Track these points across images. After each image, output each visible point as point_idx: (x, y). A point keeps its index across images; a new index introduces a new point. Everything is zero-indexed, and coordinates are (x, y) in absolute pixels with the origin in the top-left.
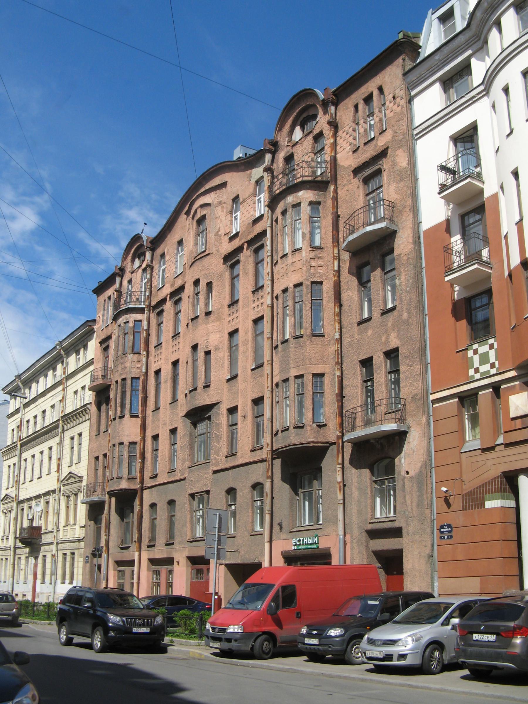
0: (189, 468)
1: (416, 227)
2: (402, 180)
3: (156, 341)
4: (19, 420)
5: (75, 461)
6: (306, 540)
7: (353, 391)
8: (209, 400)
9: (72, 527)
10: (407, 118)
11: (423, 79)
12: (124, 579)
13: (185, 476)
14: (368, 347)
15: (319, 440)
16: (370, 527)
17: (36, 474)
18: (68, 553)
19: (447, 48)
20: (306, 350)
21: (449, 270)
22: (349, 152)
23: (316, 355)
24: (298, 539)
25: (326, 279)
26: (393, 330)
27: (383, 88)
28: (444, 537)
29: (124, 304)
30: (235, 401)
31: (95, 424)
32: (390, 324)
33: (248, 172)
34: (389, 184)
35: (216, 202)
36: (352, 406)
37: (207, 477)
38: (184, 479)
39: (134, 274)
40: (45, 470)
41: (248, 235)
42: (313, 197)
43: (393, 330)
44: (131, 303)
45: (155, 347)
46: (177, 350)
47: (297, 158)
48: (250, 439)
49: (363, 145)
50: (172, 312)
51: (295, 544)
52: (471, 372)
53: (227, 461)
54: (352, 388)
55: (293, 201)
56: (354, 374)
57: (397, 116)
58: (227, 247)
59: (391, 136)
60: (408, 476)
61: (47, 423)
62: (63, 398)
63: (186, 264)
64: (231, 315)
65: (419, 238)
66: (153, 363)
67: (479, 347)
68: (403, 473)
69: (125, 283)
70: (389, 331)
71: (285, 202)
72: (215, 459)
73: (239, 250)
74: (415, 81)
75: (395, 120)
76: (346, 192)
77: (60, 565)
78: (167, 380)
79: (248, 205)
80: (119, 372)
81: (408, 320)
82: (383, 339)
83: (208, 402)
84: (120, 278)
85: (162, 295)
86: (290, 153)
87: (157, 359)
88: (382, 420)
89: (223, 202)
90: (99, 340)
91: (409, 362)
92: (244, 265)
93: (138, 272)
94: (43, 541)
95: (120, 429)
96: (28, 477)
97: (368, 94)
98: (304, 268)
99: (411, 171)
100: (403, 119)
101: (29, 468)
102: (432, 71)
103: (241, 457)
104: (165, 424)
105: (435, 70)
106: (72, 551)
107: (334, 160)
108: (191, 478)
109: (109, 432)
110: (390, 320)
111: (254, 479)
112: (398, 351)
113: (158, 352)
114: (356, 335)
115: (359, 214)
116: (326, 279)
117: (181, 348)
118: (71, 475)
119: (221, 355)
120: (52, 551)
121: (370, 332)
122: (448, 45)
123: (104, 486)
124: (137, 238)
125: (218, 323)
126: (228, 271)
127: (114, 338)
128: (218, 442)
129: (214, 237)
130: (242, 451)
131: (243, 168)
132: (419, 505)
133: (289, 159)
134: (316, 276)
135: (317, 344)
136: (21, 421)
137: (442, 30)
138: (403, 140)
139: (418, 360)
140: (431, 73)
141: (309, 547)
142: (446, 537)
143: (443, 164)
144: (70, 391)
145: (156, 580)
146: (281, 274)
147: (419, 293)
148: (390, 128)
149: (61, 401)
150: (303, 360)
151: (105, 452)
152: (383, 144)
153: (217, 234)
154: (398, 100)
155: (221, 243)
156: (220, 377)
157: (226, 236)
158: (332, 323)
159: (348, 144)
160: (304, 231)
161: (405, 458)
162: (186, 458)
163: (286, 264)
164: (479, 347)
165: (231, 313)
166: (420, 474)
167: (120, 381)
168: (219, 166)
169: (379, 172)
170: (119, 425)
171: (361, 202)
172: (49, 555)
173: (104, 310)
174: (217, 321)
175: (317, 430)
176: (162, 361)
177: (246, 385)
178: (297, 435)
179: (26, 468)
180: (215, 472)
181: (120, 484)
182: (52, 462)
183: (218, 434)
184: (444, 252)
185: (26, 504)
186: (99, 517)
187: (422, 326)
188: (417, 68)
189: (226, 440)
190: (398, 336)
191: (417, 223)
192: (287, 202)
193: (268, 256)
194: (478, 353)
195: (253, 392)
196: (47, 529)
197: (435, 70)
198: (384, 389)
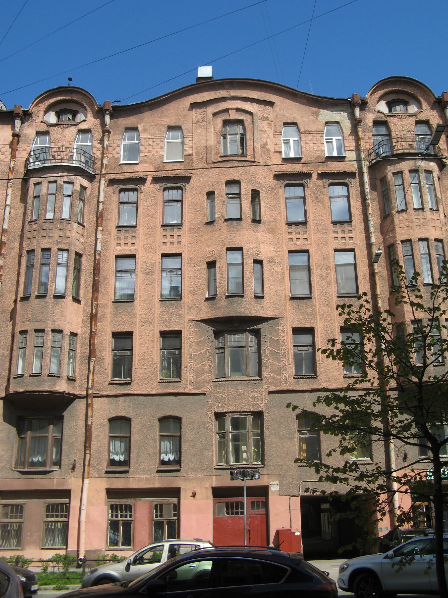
12: (21, 517)
44: (63, 161)
83: (262, 314)
131: (305, 101)
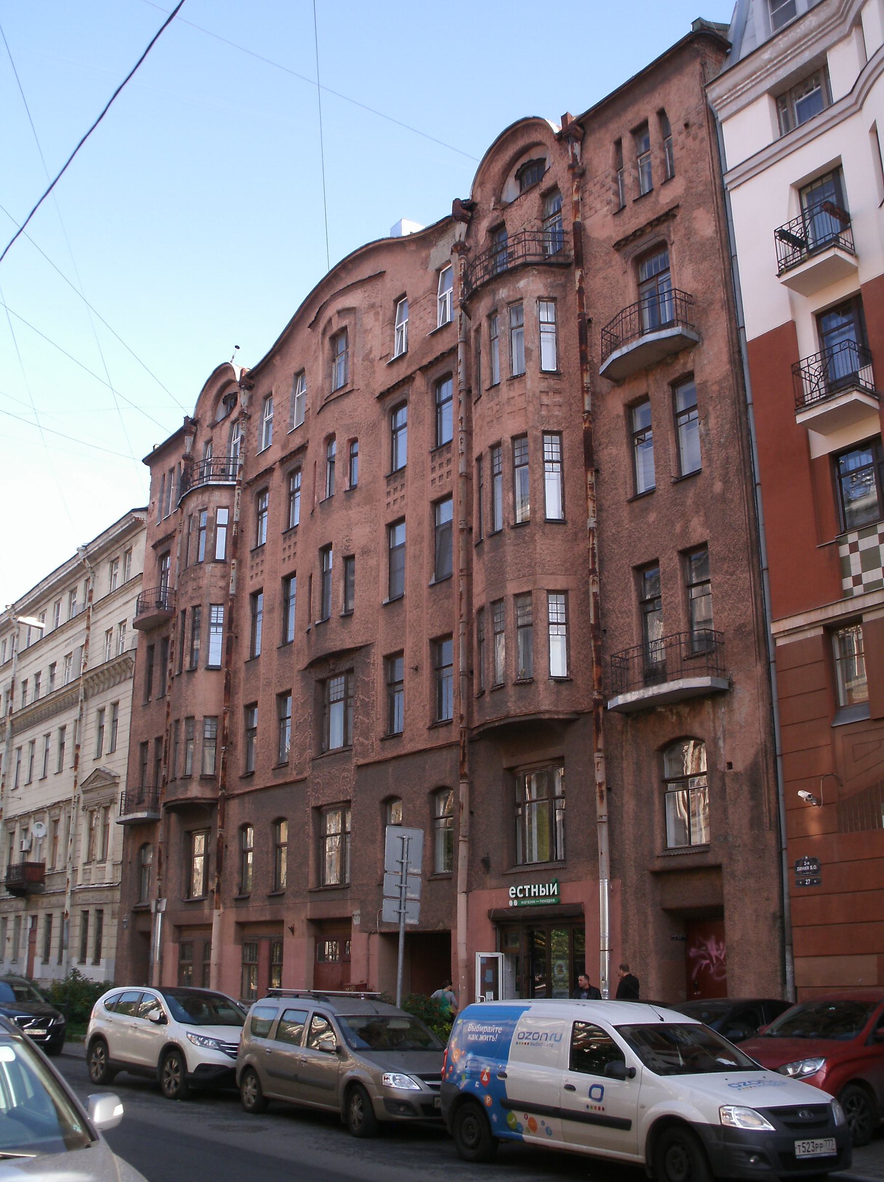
0: (313, 760)
1: (734, 336)
2: (704, 259)
3: (254, 543)
4: (10, 680)
5: (106, 750)
7: (622, 621)
8: (350, 640)
9: (98, 866)
10: (712, 158)
13: (305, 775)
14: (649, 542)
16: (658, 865)
17: (38, 773)
18: (92, 910)
19: (786, 39)
20: (535, 550)
21: (801, 404)
22: (606, 216)
24: (522, 887)
25: (568, 427)
26: (697, 512)
29: (200, 479)
30: (399, 641)
31: (143, 686)
32: (689, 502)
33: (424, 254)
34: (682, 265)
35: (365, 304)
36: (620, 647)
37: (347, 777)
38: (304, 780)
39: (217, 430)
40: (53, 766)
41: (423, 358)
42: (543, 289)
43: (697, 512)
45: (252, 551)
46: (292, 555)
47: (510, 229)
48: (428, 707)
49: (631, 202)
50: (284, 491)
52: (848, 583)
53: (383, 749)
54: (619, 615)
55: (509, 296)
56: (623, 590)
58: (384, 379)
59: (684, 187)
60: (731, 770)
61: (59, 683)
62: (87, 641)
64: (392, 493)
65: (740, 352)
66: (248, 578)
69: (201, 445)
70: (688, 513)
71: (494, 299)
72: (362, 744)
73: (408, 380)
75: (689, 161)
76: (602, 281)
77: (77, 931)
78: (273, 608)
79: (422, 308)
80: (189, 594)
81: (724, 494)
82: (678, 528)
83: (349, 644)
84: (192, 438)
85: (266, 464)
86: (498, 221)
87: (255, 572)
88: (682, 671)
89: (378, 304)
90: (152, 543)
91: (729, 567)
92: (415, 408)
93: (224, 426)
94: (47, 889)
95: (188, 693)
96: (24, 777)
97: (639, 122)
98: (531, 408)
100: (704, 160)
101: (25, 762)
103: (411, 740)
104: (269, 684)
105: (762, 77)
106: (99, 907)
107: (579, 229)
108: (317, 778)
109: (168, 698)
110: (691, 495)
111: (433, 779)
113: (258, 560)
114: (626, 522)
115: (631, 314)
116: (568, 427)
117: (299, 552)
118: (98, 774)
119: (373, 562)
120: (64, 906)
121: (652, 517)
122: (786, 33)
123: (156, 793)
124: (224, 370)
125: (368, 507)
126: (386, 419)
127: (178, 538)
128: (367, 715)
129: (361, 362)
130: (411, 730)
132: (755, 822)
133: (497, 230)
136: (13, 682)
137: (770, 14)
138: (704, 193)
139: (745, 562)
140: (754, 83)
141: (542, 901)
143: (783, 228)
144: (98, 633)
145: (250, 959)
146: (488, 419)
147: (743, 447)
148: (681, 174)
149: (82, 646)
150: (530, 565)
151: (160, 734)
153: (366, 358)
154: (693, 130)
155: (374, 372)
156: (372, 600)
158: (581, 502)
159: (605, 202)
160: (529, 345)
161: (724, 741)
162: (308, 744)
163: (496, 401)
165: (392, 490)
166: (754, 767)
167: (189, 609)
169: (662, 246)
170: (187, 686)
171: (631, 296)
172: (57, 914)
173: (162, 492)
174: (366, 504)
175: (556, 690)
176: (265, 575)
177: (420, 614)
179: (19, 762)
180: (359, 767)
181: (186, 790)
182: (66, 752)
183: (367, 700)
184: (793, 373)
185: (18, 825)
187: (751, 505)
189: (381, 712)
190: (706, 522)
191: (736, 327)
192: (497, 298)
196: (54, 868)
198: (681, 616)
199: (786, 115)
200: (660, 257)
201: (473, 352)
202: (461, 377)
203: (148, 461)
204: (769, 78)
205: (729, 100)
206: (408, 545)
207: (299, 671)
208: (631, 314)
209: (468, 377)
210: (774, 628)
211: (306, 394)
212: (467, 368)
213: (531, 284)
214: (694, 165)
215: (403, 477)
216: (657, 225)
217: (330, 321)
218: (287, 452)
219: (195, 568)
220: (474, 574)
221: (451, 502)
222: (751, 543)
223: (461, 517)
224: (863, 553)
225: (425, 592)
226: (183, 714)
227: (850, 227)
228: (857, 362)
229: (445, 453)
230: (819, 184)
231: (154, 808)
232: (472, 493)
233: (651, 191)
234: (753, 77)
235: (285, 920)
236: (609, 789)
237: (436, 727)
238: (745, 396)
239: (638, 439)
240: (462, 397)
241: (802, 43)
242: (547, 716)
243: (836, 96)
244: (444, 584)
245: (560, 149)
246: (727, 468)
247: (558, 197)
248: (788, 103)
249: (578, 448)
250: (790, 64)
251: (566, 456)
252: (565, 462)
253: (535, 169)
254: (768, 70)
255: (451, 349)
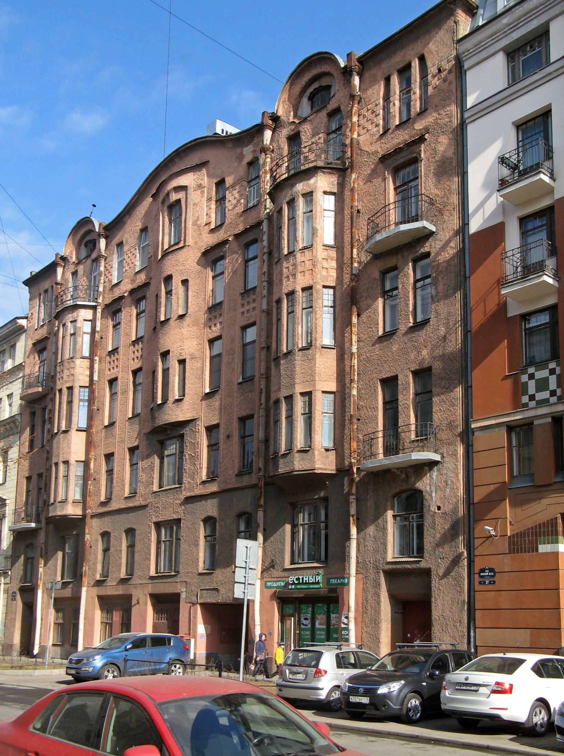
6: (307, 579)
11: (482, 48)
15: (328, 467)
19: (521, 9)
23: (327, 371)
27: (426, 58)
28: (485, 583)
32: (421, 340)
33: (238, 151)
38: (145, 506)
51: (292, 582)
57: (442, 94)
60: (439, 511)
63: (153, 257)
67: (536, 371)
68: (434, 508)
72: (189, 483)
74: (471, 51)
75: (439, 98)
83: (181, 418)
91: (445, 384)
99: (458, 161)
102: (496, 38)
104: (123, 441)
105: (500, 37)
112: (431, 370)
121: (395, 348)
124: (86, 222)
134: (329, 279)
135: (327, 358)
140: (493, 41)
141: (311, 586)
142: (487, 582)
148: (432, 108)
151: (40, 472)
152: (421, 128)
157: (206, 227)
164: (536, 371)
168: (199, 141)
174: (193, 325)
178: (303, 459)
181: (63, 509)
186: (347, 544)
188: (479, 32)
193: (264, 253)
194: (534, 379)
195: (240, 409)
197: (500, 37)
199: (513, 67)
200: (412, 167)
201: (275, 227)
202: (265, 243)
203: (27, 283)
204: (505, 38)
205: (473, 53)
206: (224, 355)
207: (144, 434)
208: (386, 212)
209: (270, 242)
210: (473, 426)
211: (148, 245)
212: (270, 236)
213: (319, 182)
214: (443, 102)
215: (221, 309)
216: (411, 146)
217: (168, 194)
218: (135, 286)
219: (68, 361)
220: (272, 378)
221: (255, 327)
222: (462, 368)
223: (263, 339)
224: (537, 381)
225: (235, 387)
226: (61, 459)
227: (552, 157)
228: (546, 253)
229: (251, 295)
230: (532, 122)
231: (38, 521)
232: (272, 325)
233: (408, 120)
234: (493, 37)
235: (133, 594)
236: (358, 519)
237: (241, 475)
238: (465, 272)
239: (387, 295)
240: (265, 257)
241: (533, 13)
242: (319, 471)
243: (553, 59)
244: (249, 383)
245: (344, 80)
246: (448, 319)
247: (339, 116)
248: (516, 59)
249: (346, 298)
250: (522, 29)
251: (338, 303)
252: (337, 307)
253: (324, 93)
254: (505, 32)
255: (258, 223)
